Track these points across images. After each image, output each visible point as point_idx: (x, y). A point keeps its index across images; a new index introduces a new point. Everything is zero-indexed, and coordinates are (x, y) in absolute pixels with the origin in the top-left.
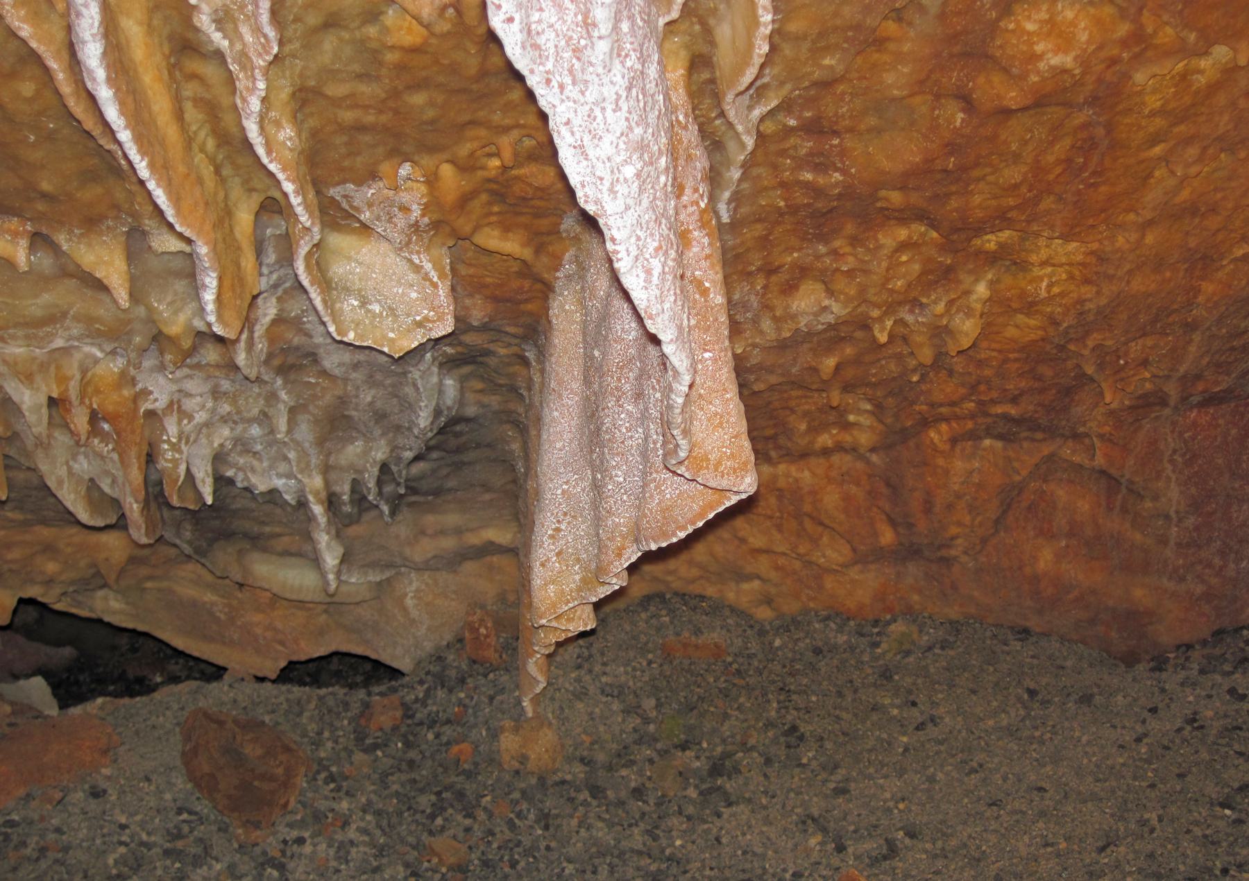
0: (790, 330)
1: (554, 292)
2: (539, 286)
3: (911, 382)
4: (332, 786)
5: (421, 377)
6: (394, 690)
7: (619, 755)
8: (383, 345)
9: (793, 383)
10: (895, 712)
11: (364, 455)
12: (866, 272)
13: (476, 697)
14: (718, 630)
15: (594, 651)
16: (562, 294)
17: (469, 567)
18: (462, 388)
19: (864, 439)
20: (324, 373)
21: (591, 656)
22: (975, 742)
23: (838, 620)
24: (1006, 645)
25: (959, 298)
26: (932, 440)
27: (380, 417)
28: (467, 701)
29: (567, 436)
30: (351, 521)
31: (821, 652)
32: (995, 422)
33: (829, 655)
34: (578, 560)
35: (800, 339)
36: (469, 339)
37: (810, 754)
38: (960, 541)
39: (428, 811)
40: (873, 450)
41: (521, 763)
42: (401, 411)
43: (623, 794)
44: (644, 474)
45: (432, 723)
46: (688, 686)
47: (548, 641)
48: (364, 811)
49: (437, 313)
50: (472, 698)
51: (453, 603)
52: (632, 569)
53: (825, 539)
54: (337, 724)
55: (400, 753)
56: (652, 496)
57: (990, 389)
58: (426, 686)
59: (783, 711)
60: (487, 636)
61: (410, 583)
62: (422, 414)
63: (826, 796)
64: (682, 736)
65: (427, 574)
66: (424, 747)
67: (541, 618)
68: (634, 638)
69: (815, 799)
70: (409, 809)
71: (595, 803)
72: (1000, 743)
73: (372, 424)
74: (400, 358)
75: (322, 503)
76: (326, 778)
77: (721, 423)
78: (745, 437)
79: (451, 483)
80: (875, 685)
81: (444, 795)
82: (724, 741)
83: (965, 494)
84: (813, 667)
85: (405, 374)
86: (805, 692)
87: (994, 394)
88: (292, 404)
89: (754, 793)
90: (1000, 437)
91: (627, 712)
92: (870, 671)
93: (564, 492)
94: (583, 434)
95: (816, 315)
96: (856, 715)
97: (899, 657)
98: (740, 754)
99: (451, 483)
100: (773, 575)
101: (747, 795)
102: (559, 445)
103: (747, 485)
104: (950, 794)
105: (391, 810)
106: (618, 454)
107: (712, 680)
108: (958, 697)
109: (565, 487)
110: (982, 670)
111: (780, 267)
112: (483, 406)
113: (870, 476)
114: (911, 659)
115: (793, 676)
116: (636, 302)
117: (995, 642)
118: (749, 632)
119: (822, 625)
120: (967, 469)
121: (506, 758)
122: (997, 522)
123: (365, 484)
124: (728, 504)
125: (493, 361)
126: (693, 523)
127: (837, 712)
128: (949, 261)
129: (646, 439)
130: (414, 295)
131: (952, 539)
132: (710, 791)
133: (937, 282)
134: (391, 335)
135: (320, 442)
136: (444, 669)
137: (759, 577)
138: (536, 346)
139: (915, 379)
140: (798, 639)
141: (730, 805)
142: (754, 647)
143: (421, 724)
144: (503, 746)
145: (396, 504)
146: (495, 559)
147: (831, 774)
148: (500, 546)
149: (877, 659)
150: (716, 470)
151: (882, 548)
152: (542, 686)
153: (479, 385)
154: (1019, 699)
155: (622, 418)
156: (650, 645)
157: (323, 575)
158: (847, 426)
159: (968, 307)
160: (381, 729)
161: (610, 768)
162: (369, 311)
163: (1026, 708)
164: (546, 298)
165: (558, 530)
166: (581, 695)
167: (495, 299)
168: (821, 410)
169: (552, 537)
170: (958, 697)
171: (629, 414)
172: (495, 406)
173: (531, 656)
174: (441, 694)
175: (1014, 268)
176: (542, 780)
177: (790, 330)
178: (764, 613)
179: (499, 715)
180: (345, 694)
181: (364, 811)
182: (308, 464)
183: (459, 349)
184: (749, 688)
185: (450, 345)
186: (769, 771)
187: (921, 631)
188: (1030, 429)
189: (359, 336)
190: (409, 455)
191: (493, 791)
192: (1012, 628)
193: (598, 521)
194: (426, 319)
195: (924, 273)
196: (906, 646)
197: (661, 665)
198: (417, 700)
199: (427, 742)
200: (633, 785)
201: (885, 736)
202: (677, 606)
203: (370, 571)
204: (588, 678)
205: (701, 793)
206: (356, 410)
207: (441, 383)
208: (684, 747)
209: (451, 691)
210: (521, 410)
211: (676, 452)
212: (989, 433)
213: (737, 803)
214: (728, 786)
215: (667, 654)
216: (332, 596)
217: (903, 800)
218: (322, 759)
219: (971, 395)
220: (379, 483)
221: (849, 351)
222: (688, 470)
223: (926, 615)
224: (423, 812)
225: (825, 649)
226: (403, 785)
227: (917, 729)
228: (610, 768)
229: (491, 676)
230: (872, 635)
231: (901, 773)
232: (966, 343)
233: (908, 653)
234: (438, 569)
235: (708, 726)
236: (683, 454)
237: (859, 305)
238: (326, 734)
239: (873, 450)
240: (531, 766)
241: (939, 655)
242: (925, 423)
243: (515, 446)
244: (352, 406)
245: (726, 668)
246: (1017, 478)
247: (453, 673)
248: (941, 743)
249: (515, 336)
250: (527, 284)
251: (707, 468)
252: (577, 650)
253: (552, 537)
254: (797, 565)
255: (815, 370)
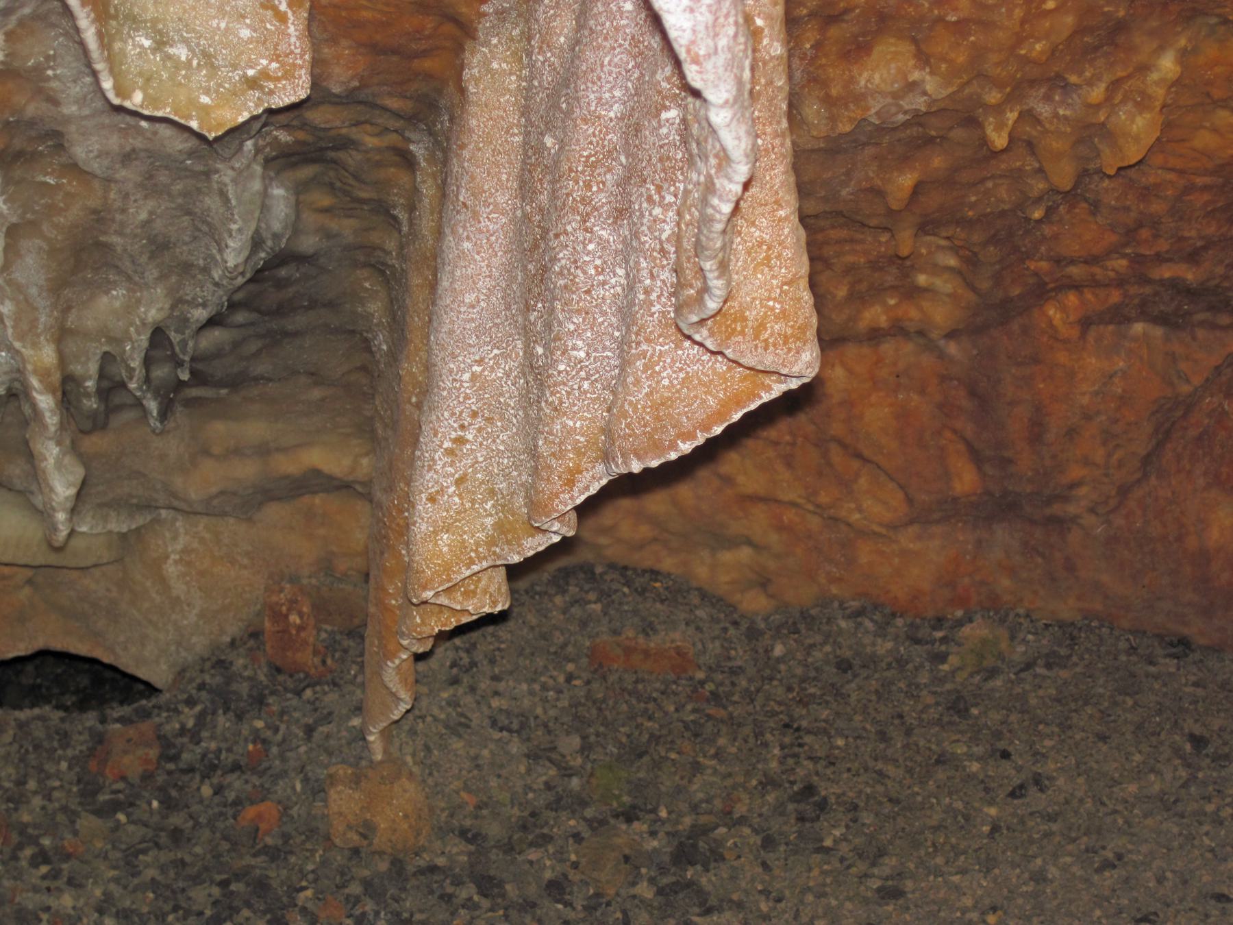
0: (851, 120)
1: (474, 38)
2: (449, 28)
3: (1028, 220)
4: (44, 869)
5: (235, 181)
6: (145, 714)
7: (524, 828)
8: (190, 117)
9: (840, 214)
10: (975, 767)
11: (126, 312)
12: (987, 25)
13: (283, 727)
14: (683, 626)
15: (479, 656)
16: (487, 43)
17: (274, 512)
18: (298, 203)
19: (940, 315)
20: (74, 168)
21: (473, 664)
22: (1109, 820)
23: (877, 617)
24: (1151, 663)
25: (1129, 77)
26: (1050, 324)
27: (159, 247)
28: (269, 733)
29: (484, 284)
30: (98, 423)
31: (850, 667)
32: (1156, 294)
33: (864, 673)
34: (492, 493)
35: (863, 139)
36: (316, 116)
37: (837, 833)
38: (1083, 491)
39: (208, 913)
40: (952, 335)
41: (364, 836)
42: (195, 238)
43: (532, 891)
44: (623, 345)
45: (209, 768)
46: (632, 718)
47: (427, 631)
48: (101, 911)
49: (283, 65)
50: (277, 730)
51: (245, 573)
52: (585, 510)
53: (863, 482)
54: (50, 767)
55: (156, 818)
56: (637, 382)
57: (1156, 236)
58: (198, 708)
59: (791, 761)
60: (301, 628)
61: (175, 538)
62: (231, 244)
63: (866, 901)
64: (625, 799)
65: (203, 521)
66: (195, 808)
67: (425, 588)
68: (544, 637)
69: (849, 905)
70: (176, 909)
71: (486, 903)
72: (1149, 822)
73: (144, 259)
74: (217, 139)
75: (54, 393)
76: (33, 857)
77: (768, 258)
78: (804, 283)
79: (262, 368)
80: (938, 722)
81: (233, 887)
82: (694, 808)
83: (1098, 413)
84: (839, 694)
85: (207, 174)
86: (825, 732)
87: (1163, 246)
88: (14, 219)
89: (746, 892)
90: (1160, 319)
91: (533, 756)
92: (930, 700)
93: (474, 377)
94: (512, 279)
95: (896, 96)
96: (910, 771)
97: (977, 678)
98: (722, 830)
99: (262, 368)
100: (773, 538)
101: (735, 897)
102: (470, 298)
103: (804, 364)
104: (1071, 901)
105: (145, 909)
106: (578, 312)
107: (672, 708)
108: (1077, 745)
109: (477, 369)
110: (1115, 704)
111: (846, 11)
112: (329, 235)
113: (943, 378)
114: (998, 682)
115: (806, 705)
116: (672, 34)
117: (1134, 658)
118: (732, 631)
119: (851, 624)
120: (1101, 371)
121: (339, 826)
122: (1147, 460)
123: (124, 361)
124: (766, 397)
125: (351, 158)
126: (707, 429)
127: (880, 765)
128: (1121, 13)
129: (630, 288)
130: (245, 33)
131: (1073, 486)
132: (676, 888)
133: (1096, 48)
134: (205, 100)
135: (56, 287)
136: (229, 680)
137: (749, 542)
138: (431, 133)
139: (1037, 214)
140: (812, 646)
141: (708, 911)
142: (740, 656)
143: (191, 770)
144: (334, 808)
145: (170, 396)
146: (317, 500)
147: (873, 864)
148: (331, 478)
149: (942, 680)
150: (756, 337)
151: (955, 500)
152: (404, 707)
153: (326, 201)
154: (1177, 751)
155: (589, 253)
156: (570, 649)
157: (44, 514)
158: (912, 293)
159: (1143, 93)
160: (123, 778)
161: (509, 848)
162: (168, 57)
163: (1189, 766)
164: (460, 48)
165: (460, 441)
166: (459, 727)
167: (376, 49)
168: (874, 265)
169: (450, 452)
170: (1077, 745)
171: (603, 244)
172: (349, 237)
173: (392, 656)
174: (223, 721)
175: (1222, 29)
176: (397, 864)
177: (851, 120)
178: (755, 603)
179: (323, 758)
180: (62, 720)
181: (101, 911)
182: (34, 323)
183: (301, 135)
184: (734, 724)
185: (286, 127)
186: (770, 857)
187: (1012, 638)
188: (1211, 308)
189: (149, 100)
190: (200, 314)
191: (316, 881)
192: (1160, 637)
193: (533, 426)
194: (265, 74)
195: (1079, 31)
196: (989, 662)
197: (588, 682)
198: (183, 731)
199: (201, 801)
200: (548, 875)
201: (959, 805)
202: (615, 586)
203: (113, 514)
204: (469, 699)
205: (660, 892)
206: (120, 233)
207: (265, 194)
208: (629, 816)
209: (240, 717)
210: (391, 245)
211: (699, 300)
212: (1144, 313)
213: (720, 910)
214: (704, 881)
215: (598, 662)
216: (59, 550)
217: (994, 909)
218: (26, 825)
219: (1126, 245)
220: (148, 362)
221: (938, 162)
222: (712, 334)
223: (1021, 611)
224: (201, 914)
225: (857, 662)
226: (163, 869)
227: (1012, 794)
228: (509, 848)
229: (308, 693)
230: (933, 642)
231: (989, 865)
232: (1133, 154)
233: (992, 673)
234: (224, 514)
235: (667, 783)
236: (712, 305)
237: (968, 83)
238: (32, 785)
239: (952, 335)
240: (379, 841)
241: (1044, 677)
242: (1041, 292)
243: (375, 308)
244: (115, 227)
245: (695, 691)
246: (1185, 389)
247: (244, 688)
248: (1052, 818)
249: (397, 115)
250: (430, 24)
251: (742, 333)
252: (451, 655)
253: (450, 452)
254: (814, 522)
255: (878, 193)
